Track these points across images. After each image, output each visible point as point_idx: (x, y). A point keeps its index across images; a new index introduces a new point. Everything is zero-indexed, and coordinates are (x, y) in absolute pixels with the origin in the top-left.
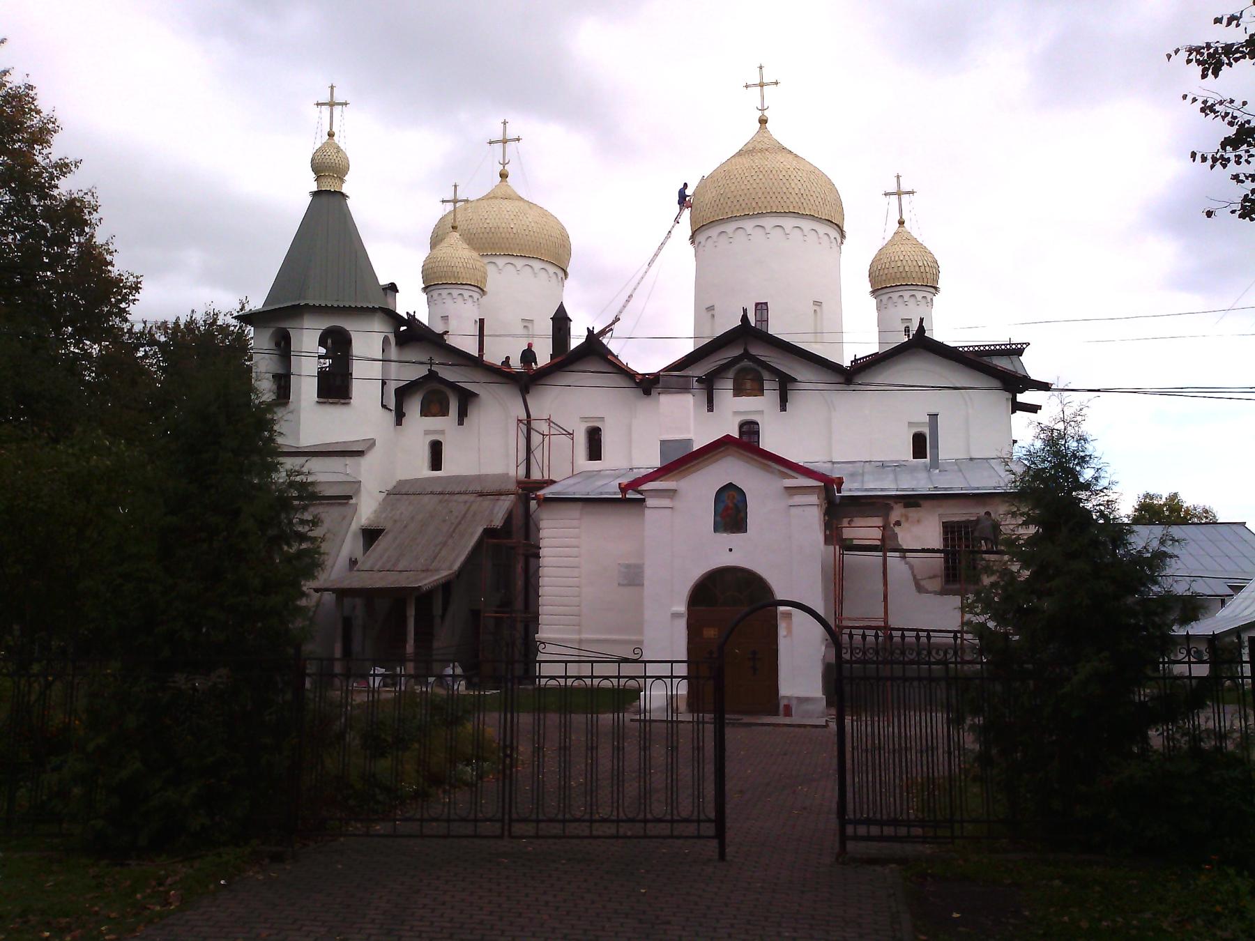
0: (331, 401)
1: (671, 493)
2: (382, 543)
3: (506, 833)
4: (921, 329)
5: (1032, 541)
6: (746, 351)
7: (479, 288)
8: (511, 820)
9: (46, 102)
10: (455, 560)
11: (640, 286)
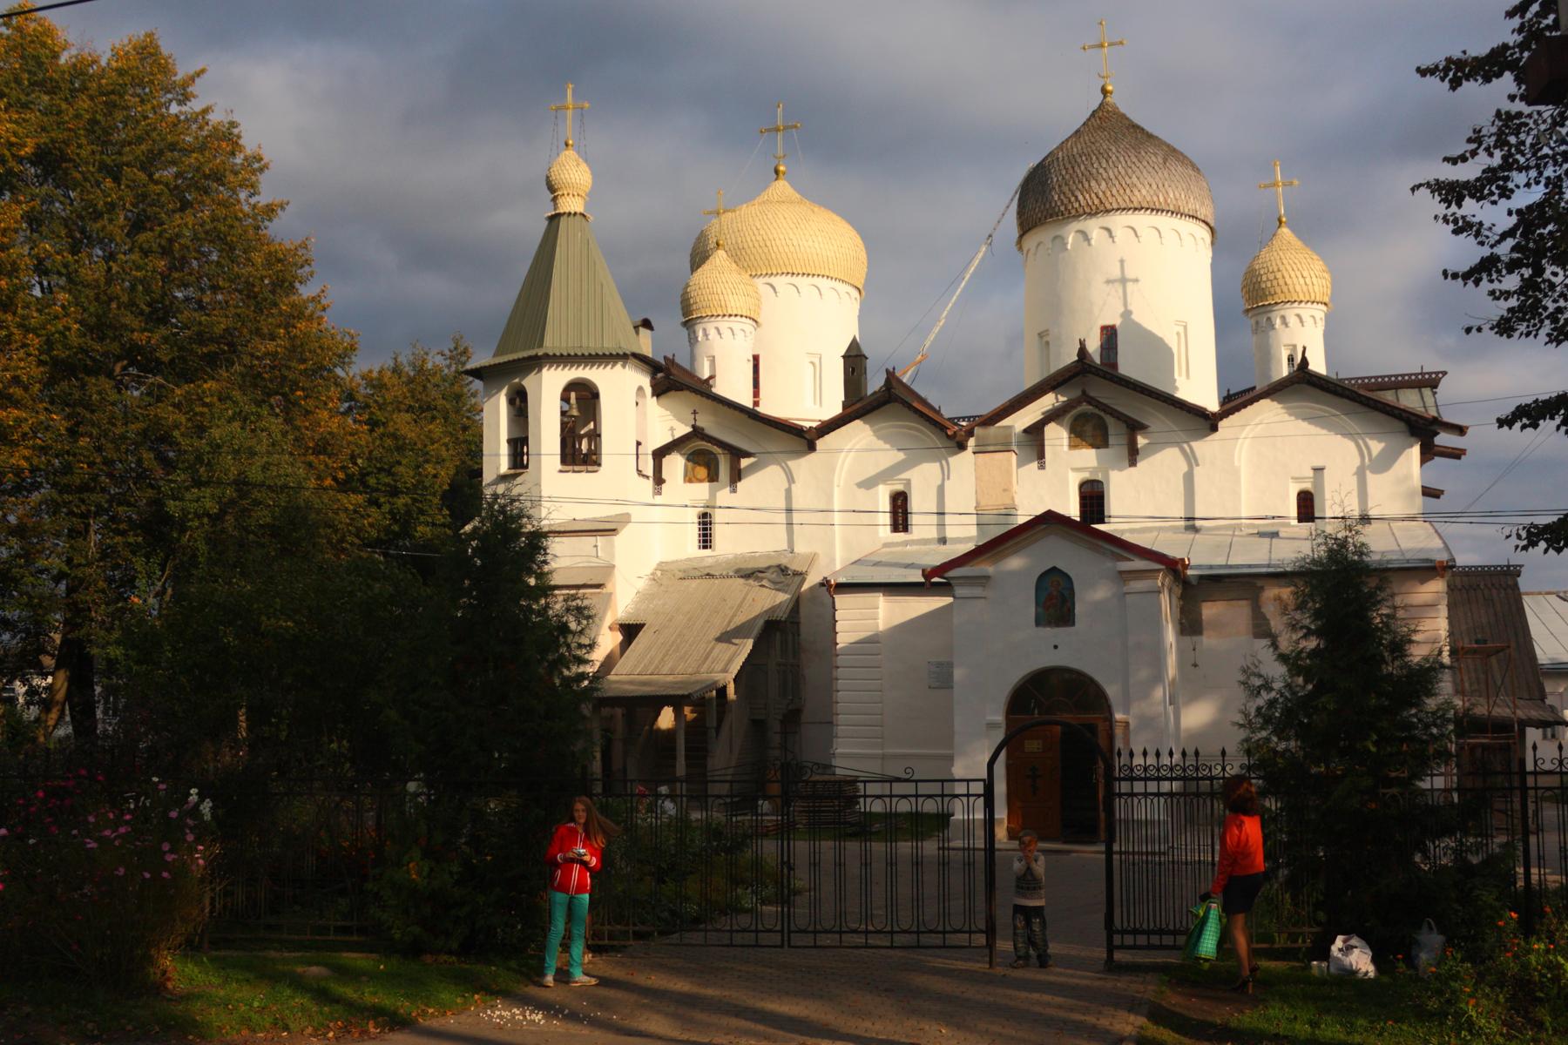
0: (576, 468)
1: (983, 580)
2: (641, 640)
3: (786, 943)
4: (1304, 361)
5: (1314, 653)
6: (1084, 393)
7: (753, 320)
8: (790, 932)
9: (251, 139)
10: (730, 661)
11: (1002, 211)
